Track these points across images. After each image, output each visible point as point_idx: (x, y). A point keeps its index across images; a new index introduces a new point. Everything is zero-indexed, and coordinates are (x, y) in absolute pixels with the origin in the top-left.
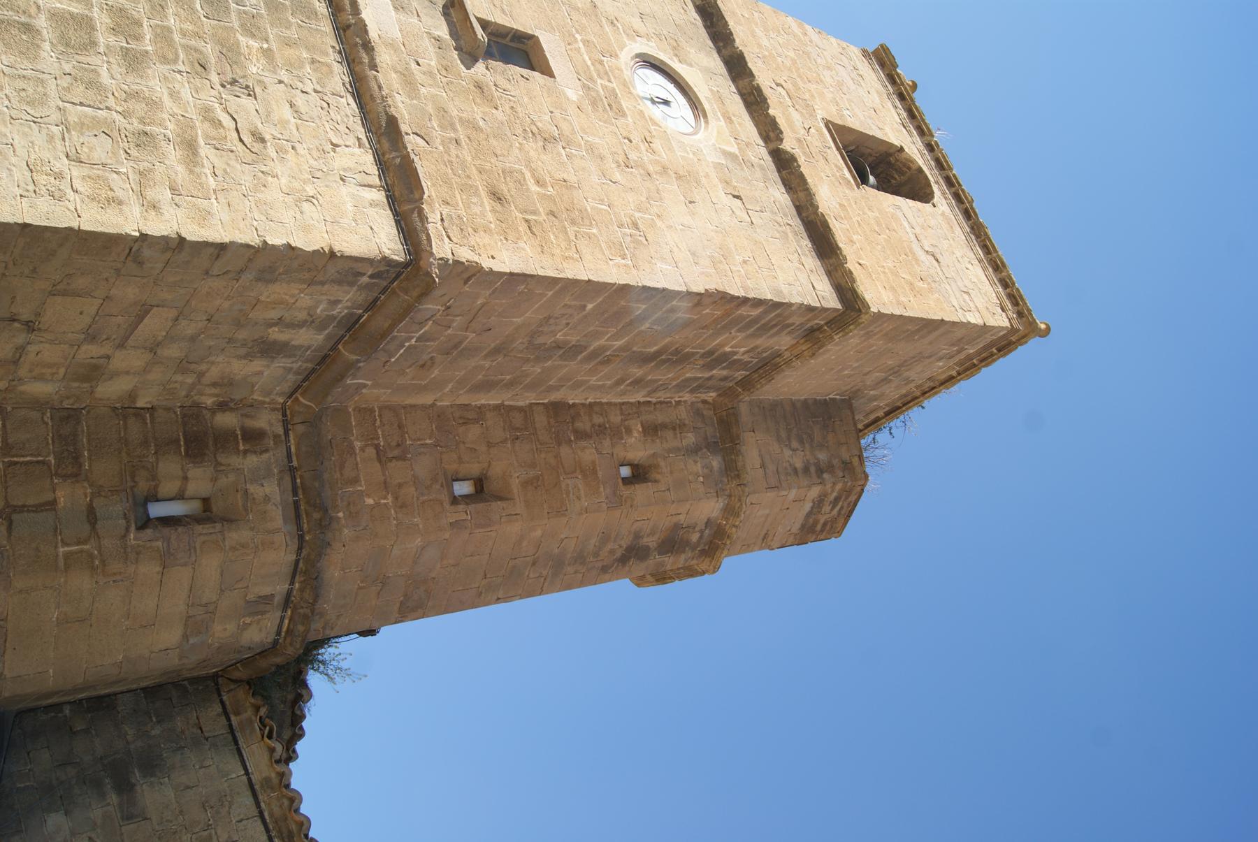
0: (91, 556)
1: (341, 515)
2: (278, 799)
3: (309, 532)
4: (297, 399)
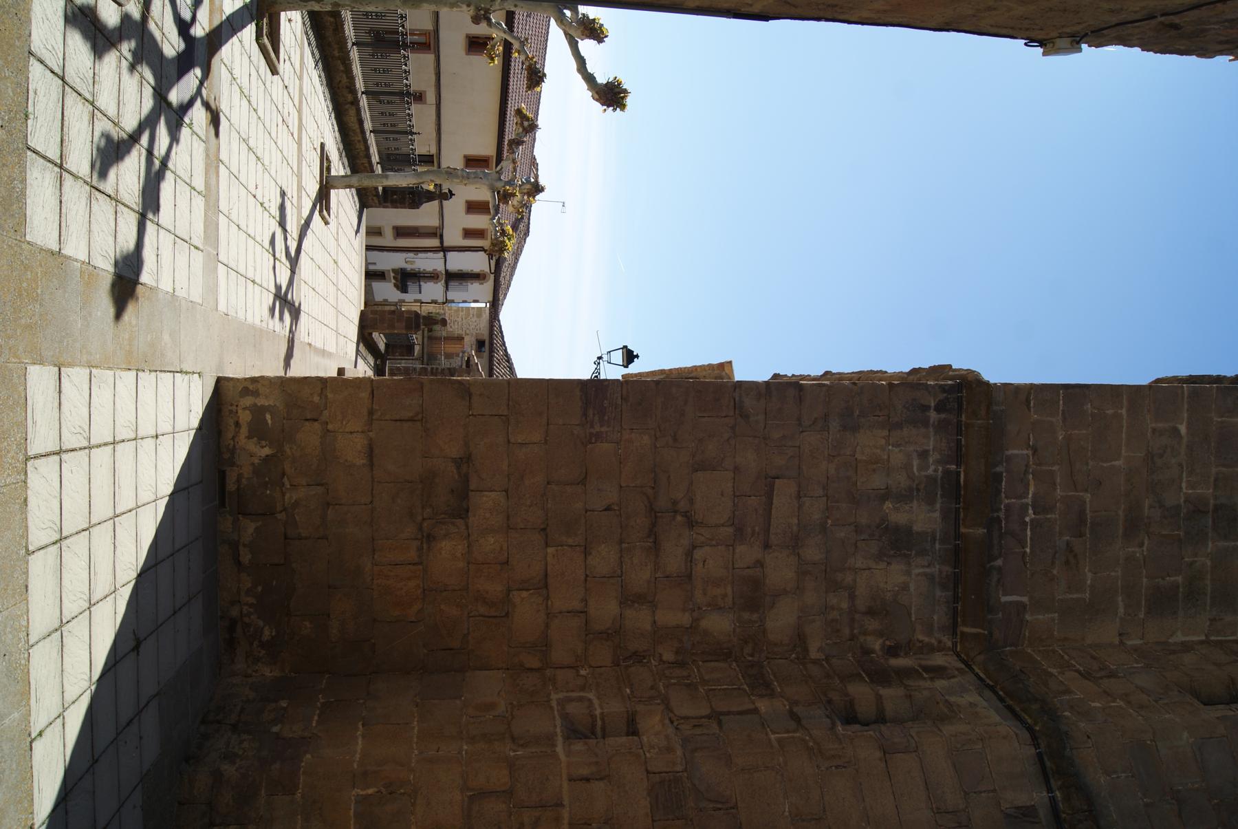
1: (1066, 713)
4: (963, 633)
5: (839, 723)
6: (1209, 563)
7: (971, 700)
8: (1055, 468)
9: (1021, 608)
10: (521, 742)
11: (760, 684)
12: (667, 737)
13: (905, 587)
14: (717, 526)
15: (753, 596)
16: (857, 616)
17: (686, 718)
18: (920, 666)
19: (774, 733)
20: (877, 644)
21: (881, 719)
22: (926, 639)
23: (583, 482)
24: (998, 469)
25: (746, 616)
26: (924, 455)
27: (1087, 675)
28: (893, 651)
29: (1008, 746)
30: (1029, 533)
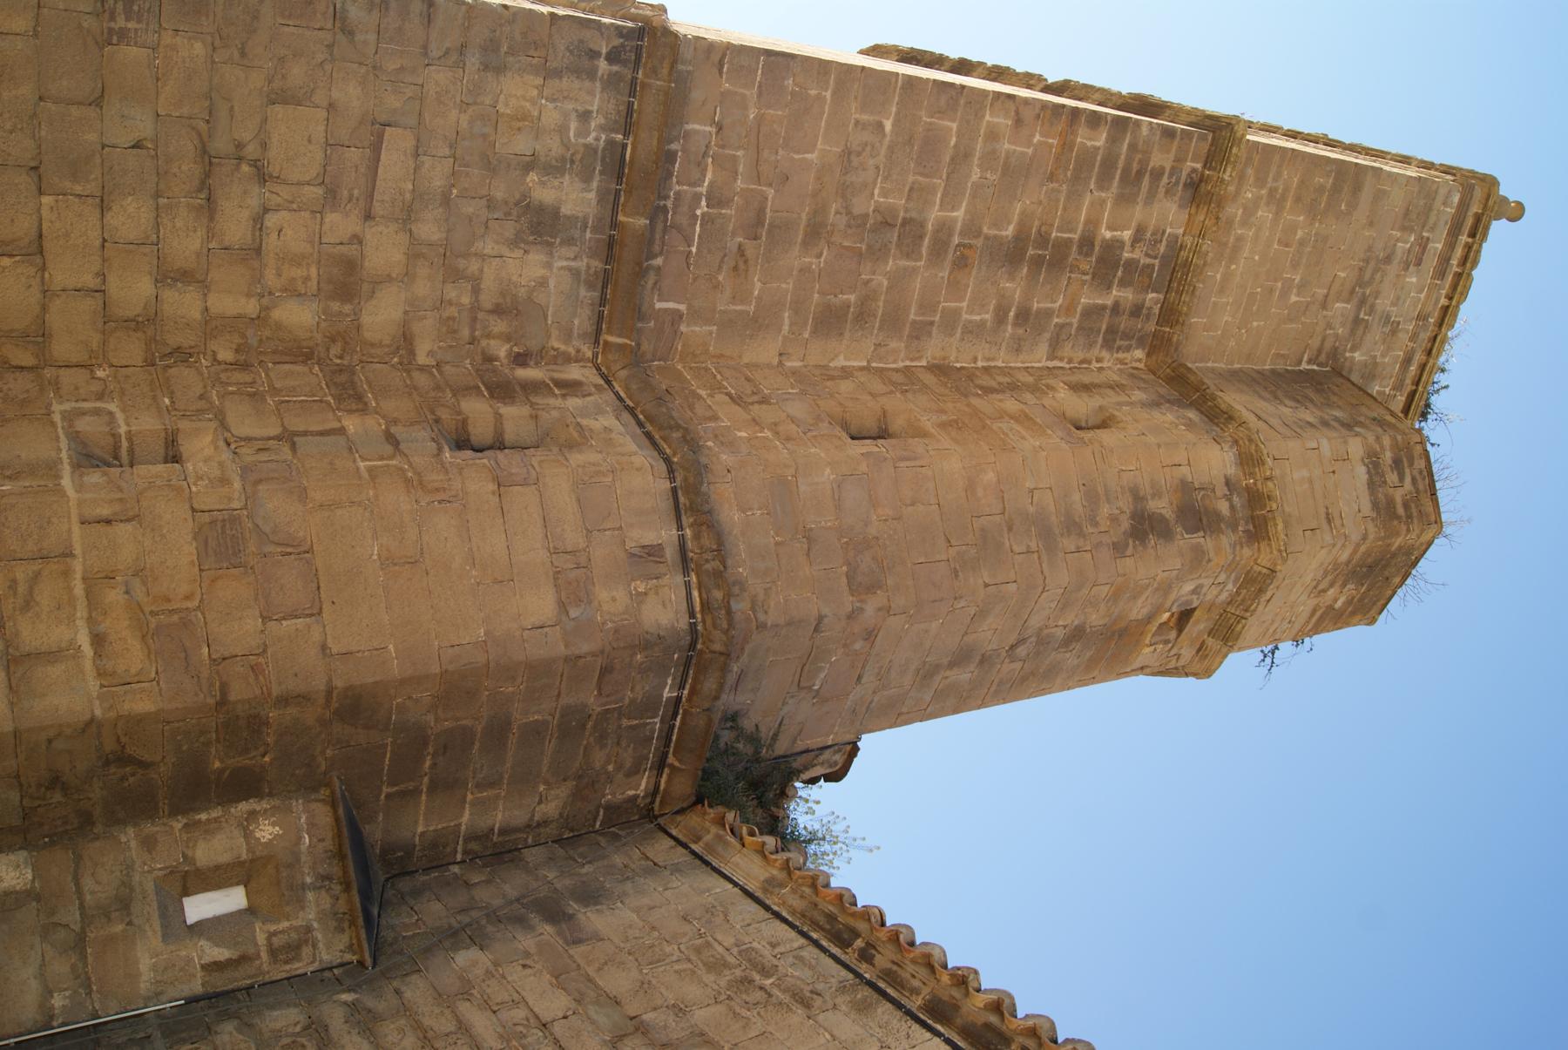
0: (401, 469)
1: (710, 444)
2: (794, 891)
3: (675, 454)
4: (606, 343)
5: (446, 448)
6: (885, 283)
7: (606, 424)
8: (740, 153)
9: (677, 317)
10: (8, 473)
11: (350, 395)
12: (221, 464)
13: (543, 283)
14: (299, 184)
15: (346, 281)
16: (480, 315)
17: (249, 439)
18: (552, 380)
19: (363, 459)
20: (502, 350)
21: (499, 445)
22: (563, 347)
23: (98, 102)
24: (673, 146)
25: (335, 306)
26: (585, 116)
27: (736, 400)
28: (521, 359)
29: (642, 478)
30: (698, 229)
